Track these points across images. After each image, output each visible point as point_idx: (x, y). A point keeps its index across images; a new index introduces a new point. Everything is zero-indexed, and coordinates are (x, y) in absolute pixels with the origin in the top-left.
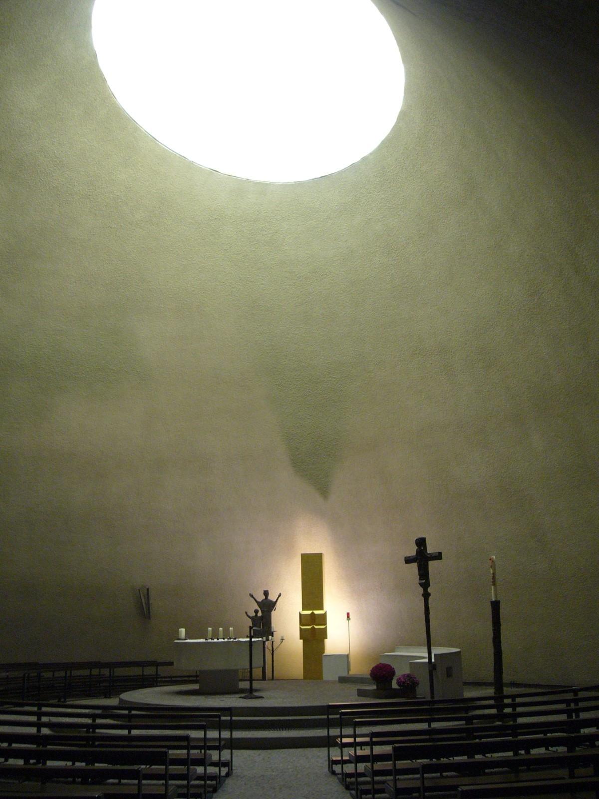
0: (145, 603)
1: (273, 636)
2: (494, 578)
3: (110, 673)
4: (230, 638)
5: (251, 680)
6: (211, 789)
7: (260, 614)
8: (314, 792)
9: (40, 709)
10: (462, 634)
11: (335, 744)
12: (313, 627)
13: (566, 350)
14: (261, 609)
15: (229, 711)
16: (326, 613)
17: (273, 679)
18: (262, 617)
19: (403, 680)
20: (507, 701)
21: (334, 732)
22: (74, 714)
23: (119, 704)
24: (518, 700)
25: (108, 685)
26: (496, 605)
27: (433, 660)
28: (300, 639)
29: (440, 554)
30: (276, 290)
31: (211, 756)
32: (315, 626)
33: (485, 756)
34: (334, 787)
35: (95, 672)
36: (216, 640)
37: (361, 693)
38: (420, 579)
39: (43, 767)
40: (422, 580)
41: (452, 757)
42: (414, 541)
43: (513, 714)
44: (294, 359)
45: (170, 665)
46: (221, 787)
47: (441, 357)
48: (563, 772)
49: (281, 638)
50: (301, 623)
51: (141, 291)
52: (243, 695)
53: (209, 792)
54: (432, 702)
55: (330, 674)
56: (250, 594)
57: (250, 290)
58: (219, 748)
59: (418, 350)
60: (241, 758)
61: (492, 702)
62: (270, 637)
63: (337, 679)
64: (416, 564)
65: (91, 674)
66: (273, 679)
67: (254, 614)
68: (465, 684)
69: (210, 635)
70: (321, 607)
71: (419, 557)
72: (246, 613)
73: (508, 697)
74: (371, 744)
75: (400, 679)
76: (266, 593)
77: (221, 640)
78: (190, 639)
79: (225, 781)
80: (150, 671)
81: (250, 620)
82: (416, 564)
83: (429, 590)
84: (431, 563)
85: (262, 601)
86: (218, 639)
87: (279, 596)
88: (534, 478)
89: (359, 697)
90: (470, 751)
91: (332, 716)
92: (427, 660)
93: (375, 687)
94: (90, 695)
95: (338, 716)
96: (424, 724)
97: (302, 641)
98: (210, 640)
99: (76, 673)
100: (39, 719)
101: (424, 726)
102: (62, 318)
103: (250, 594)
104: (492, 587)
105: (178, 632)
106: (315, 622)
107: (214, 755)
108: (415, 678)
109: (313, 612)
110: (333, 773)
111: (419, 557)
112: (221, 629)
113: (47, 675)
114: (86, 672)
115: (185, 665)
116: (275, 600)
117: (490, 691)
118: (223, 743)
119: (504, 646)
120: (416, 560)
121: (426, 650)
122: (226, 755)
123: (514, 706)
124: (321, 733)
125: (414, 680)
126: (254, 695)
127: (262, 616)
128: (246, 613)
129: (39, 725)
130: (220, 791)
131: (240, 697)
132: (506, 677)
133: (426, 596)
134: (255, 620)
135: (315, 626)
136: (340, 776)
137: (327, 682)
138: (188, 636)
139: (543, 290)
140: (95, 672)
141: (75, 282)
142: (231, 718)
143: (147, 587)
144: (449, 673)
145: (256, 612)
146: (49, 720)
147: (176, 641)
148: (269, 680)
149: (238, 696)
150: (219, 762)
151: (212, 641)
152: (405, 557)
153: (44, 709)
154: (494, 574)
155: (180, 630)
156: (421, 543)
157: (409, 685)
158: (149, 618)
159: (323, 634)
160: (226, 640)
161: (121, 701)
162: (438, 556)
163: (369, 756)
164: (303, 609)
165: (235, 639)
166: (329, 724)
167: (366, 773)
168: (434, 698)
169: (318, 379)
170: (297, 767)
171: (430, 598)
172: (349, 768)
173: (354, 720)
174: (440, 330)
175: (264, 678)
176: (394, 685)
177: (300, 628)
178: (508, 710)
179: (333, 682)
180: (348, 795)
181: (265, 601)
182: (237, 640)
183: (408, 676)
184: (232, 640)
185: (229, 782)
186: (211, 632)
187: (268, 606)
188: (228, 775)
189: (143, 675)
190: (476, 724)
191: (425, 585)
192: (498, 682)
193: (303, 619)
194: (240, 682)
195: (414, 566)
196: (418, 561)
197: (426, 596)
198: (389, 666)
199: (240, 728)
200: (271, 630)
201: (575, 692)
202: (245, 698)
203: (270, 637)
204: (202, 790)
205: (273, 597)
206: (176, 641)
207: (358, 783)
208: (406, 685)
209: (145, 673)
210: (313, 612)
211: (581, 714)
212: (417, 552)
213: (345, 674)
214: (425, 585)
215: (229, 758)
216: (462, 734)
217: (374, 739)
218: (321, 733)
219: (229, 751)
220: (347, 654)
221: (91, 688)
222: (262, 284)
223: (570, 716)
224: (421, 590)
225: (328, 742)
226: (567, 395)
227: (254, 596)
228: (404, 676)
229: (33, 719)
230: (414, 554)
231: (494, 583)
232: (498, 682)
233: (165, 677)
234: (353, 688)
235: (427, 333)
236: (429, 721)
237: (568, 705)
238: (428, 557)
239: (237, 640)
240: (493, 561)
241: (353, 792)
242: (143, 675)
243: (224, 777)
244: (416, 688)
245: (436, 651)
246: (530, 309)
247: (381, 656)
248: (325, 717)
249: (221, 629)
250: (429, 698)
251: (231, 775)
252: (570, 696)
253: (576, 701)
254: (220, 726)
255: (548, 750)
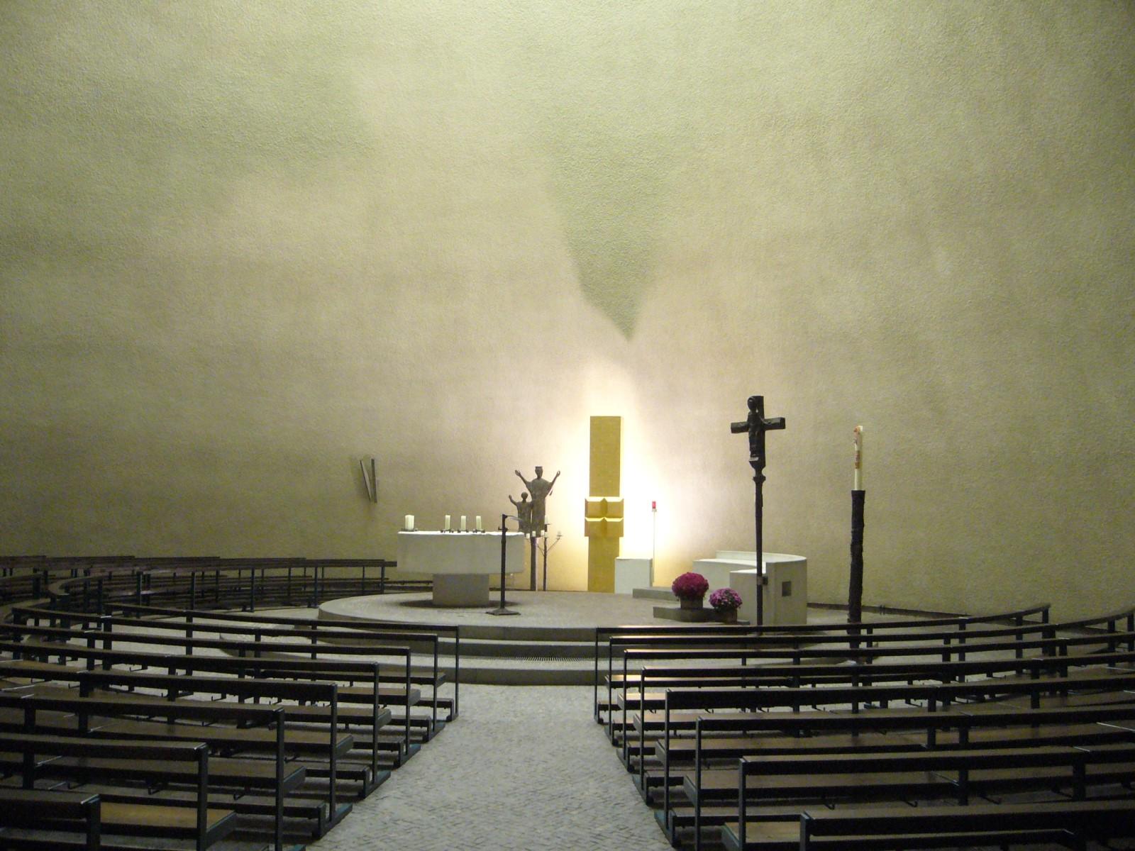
0: (370, 480)
1: (546, 531)
2: (859, 457)
3: (323, 573)
4: (476, 531)
5: (503, 589)
6: (420, 738)
7: (529, 499)
8: (566, 747)
9: (189, 620)
10: (807, 537)
11: (603, 683)
12: (604, 520)
13: (996, 123)
14: (531, 492)
15: (454, 630)
16: (623, 501)
17: (544, 590)
18: (532, 505)
19: (718, 597)
20: (864, 632)
21: (603, 665)
22: (239, 628)
23: (319, 618)
24: (876, 632)
25: (313, 590)
26: (859, 498)
27: (764, 571)
28: (586, 535)
29: (783, 420)
30: (563, 21)
31: (418, 692)
32: (606, 518)
33: (816, 708)
34: (599, 740)
35: (298, 572)
36: (456, 533)
37: (659, 613)
38: (751, 456)
39: (961, 685)
40: (754, 457)
41: (766, 707)
42: (747, 403)
43: (311, 647)
44: (588, 128)
45: (392, 566)
46: (434, 736)
47: (808, 131)
48: (920, 737)
49: (557, 534)
50: (588, 514)
51: (360, 19)
52: (491, 610)
53: (413, 742)
54: (760, 630)
55: (624, 584)
56: (516, 471)
57: (525, 21)
58: (433, 682)
59: (774, 118)
60: (472, 697)
61: (844, 633)
62: (543, 532)
63: (631, 592)
64: (748, 433)
65: (289, 576)
66: (544, 590)
67: (521, 500)
68: (810, 605)
69: (448, 526)
70: (616, 492)
71: (751, 424)
72: (510, 497)
73: (865, 626)
74: (641, 686)
75: (714, 595)
76: (539, 471)
77: (463, 533)
78: (421, 530)
79: (444, 726)
80: (373, 573)
81: (515, 507)
82: (748, 433)
83: (765, 472)
84: (768, 433)
85: (533, 481)
86: (459, 532)
87: (558, 475)
88: (934, 317)
89: (655, 619)
90: (794, 700)
91: (610, 642)
92: (755, 571)
93: (678, 605)
94: (287, 603)
95: (607, 644)
96: (935, 656)
97: (587, 538)
98: (447, 533)
99: (271, 572)
100: (189, 634)
101: (735, 663)
102: (242, 60)
103: (516, 471)
104: (856, 471)
105: (403, 521)
106: (606, 512)
107: (426, 692)
108: (736, 595)
109: (604, 500)
110: (600, 721)
111: (751, 424)
112: (478, 517)
113: (233, 574)
114: (283, 572)
115: (410, 566)
116: (551, 481)
117: (843, 618)
118: (440, 675)
119: (866, 555)
120: (748, 428)
121: (755, 557)
122: (446, 691)
123: (869, 640)
124: (587, 665)
125: (734, 598)
126: (507, 611)
127: (532, 502)
128: (510, 497)
129: (189, 644)
130: (433, 741)
131: (487, 613)
132: (867, 598)
133: (759, 480)
134: (522, 507)
135: (606, 518)
136: (608, 727)
137: (619, 596)
138: (418, 526)
139: (969, 25)
140: (298, 572)
141: (261, 4)
142: (457, 641)
143: (372, 458)
144: (786, 590)
145: (524, 496)
146: (221, 637)
147: (400, 533)
148: (539, 590)
149: (484, 610)
150: (434, 701)
151: (451, 534)
152: (732, 424)
153: (196, 621)
154: (859, 452)
155: (406, 516)
156: (756, 404)
157: (727, 606)
158: (376, 501)
159: (618, 530)
160: (471, 533)
161: (321, 612)
162: (781, 424)
163: (639, 701)
164: (592, 493)
165: (484, 532)
166: (596, 654)
167: (634, 725)
168: (762, 624)
169: (624, 160)
170: (550, 711)
171: (765, 484)
172: (617, 717)
173: (625, 651)
174: (809, 88)
175: (533, 588)
176: (707, 604)
177: (586, 520)
178: (863, 645)
179: (625, 596)
180: (615, 754)
181: (537, 481)
182: (486, 533)
183: (727, 591)
184: (479, 533)
185: (449, 728)
186: (449, 522)
187: (540, 489)
188: (449, 719)
189: (363, 578)
190: (806, 663)
191: (759, 465)
192: (855, 606)
193: (589, 510)
194: (491, 593)
195: (745, 436)
196: (750, 430)
197: (759, 480)
198: (701, 577)
199: (483, 655)
200: (544, 522)
201: (962, 624)
202: (493, 614)
203: (543, 532)
204: (401, 739)
205: (548, 477)
206: (400, 533)
207: (627, 738)
208: (723, 604)
209: (366, 576)
210: (604, 500)
211: (1025, 651)
212: (749, 416)
213: (644, 586)
214: (759, 465)
215: (452, 696)
216: (788, 677)
217: (647, 679)
218: (587, 665)
219: (454, 685)
220: (649, 558)
221: (290, 594)
222: (543, 12)
223: (946, 658)
224: (753, 472)
225: (594, 679)
226: (992, 192)
227: (522, 474)
228: (720, 591)
229: (182, 634)
230: (745, 419)
231: (858, 465)
232: (855, 606)
233: (395, 582)
234: (650, 605)
235: (788, 93)
236: (744, 656)
237: (947, 642)
238: (764, 424)
239: (486, 533)
240: (859, 433)
241: (621, 750)
242: (363, 578)
243: (443, 721)
244: (738, 609)
245: (768, 558)
246: (946, 57)
247: (695, 562)
248: (593, 644)
249: (478, 517)
250: (754, 624)
251: (454, 719)
252: (954, 629)
253: (962, 637)
254: (438, 650)
255: (910, 704)
